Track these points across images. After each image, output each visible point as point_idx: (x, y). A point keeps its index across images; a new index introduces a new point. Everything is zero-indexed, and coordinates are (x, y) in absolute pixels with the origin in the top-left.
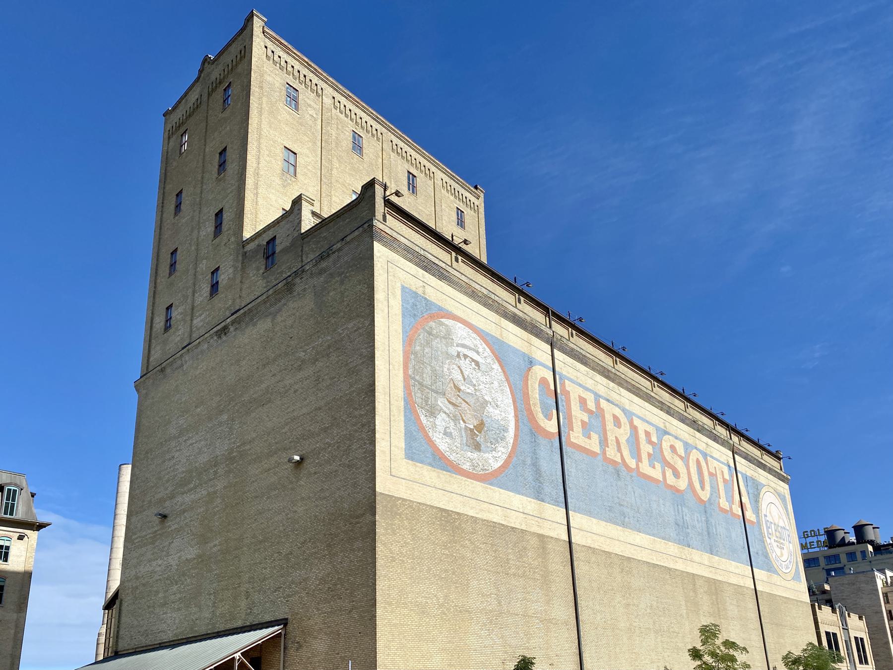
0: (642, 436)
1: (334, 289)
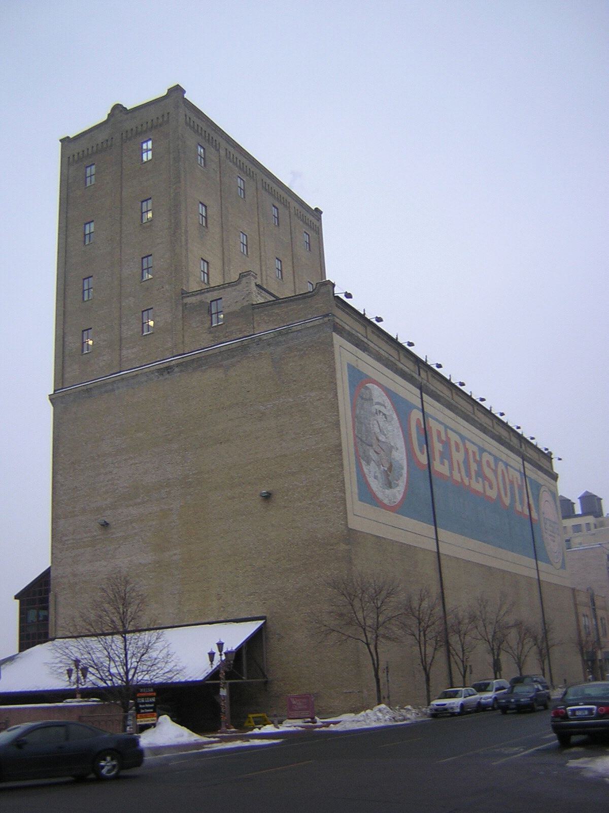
0: (471, 453)
1: (294, 361)
